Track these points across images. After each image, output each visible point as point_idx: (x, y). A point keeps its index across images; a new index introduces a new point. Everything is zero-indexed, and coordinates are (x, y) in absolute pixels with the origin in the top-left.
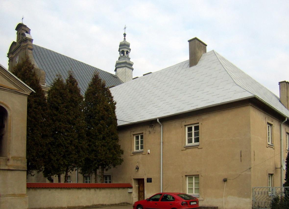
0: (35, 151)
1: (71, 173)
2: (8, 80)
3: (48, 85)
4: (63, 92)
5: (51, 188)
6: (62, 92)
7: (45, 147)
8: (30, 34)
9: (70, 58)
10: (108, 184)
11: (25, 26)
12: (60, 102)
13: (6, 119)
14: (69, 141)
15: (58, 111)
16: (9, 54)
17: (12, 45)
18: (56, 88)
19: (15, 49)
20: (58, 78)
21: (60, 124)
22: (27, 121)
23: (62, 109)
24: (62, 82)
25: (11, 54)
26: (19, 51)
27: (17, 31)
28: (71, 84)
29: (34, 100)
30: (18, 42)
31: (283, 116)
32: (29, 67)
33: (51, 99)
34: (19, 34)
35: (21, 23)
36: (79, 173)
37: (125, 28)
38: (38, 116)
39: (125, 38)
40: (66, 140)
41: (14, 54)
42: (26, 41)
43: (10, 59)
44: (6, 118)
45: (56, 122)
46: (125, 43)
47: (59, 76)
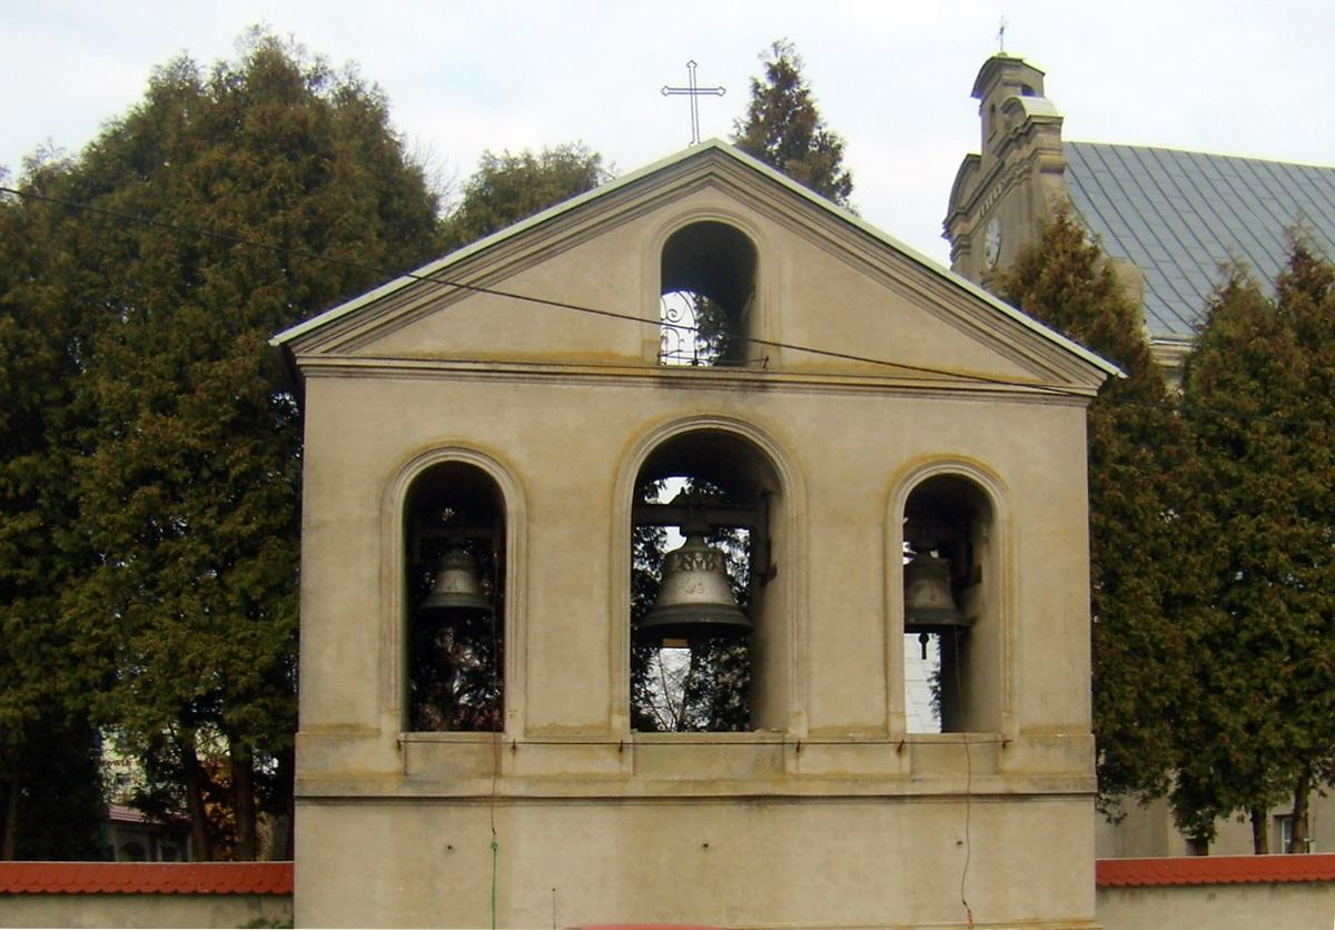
0: (1129, 688)
1: (1322, 794)
3: (1159, 334)
4: (1265, 347)
5: (1220, 884)
6: (1259, 351)
7: (1181, 663)
8: (1041, 94)
9: (1264, 164)
11: (1018, 64)
12: (1253, 406)
13: (987, 540)
14: (1313, 617)
15: (1242, 460)
16: (949, 224)
18: (1220, 336)
19: (979, 188)
20: (1227, 281)
21: (1259, 530)
23: (1265, 442)
24: (1253, 292)
25: (959, 217)
26: (999, 196)
27: (979, 102)
28: (1305, 294)
29: (1115, 421)
30: (992, 150)
32: (1074, 255)
33: (1201, 400)
34: (993, 108)
35: (995, 55)
36: (1199, 844)
38: (1140, 500)
40: (1295, 609)
41: (976, 212)
42: (1027, 133)
43: (957, 243)
44: (988, 531)
45: (1235, 520)
47: (1231, 266)
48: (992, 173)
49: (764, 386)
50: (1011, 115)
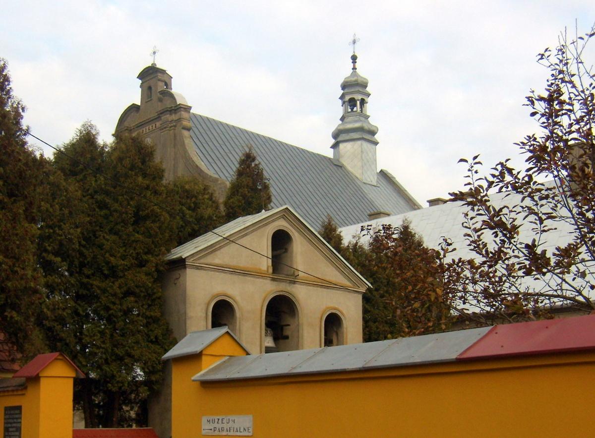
2: (342, 273)
10: (135, 430)
11: (163, 72)
17: (129, 110)
27: (140, 81)
37: (354, 42)
39: (354, 66)
42: (175, 110)
46: (356, 81)
48: (150, 120)
49: (294, 282)
50: (164, 96)
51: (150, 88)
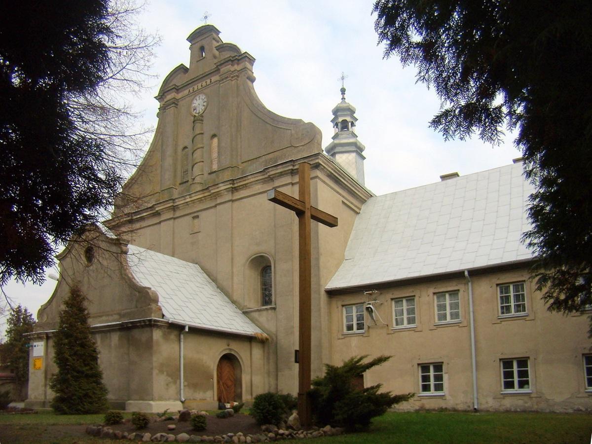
17: (175, 72)
22: (311, 305)
25: (174, 90)
27: (191, 44)
31: (516, 264)
37: (343, 78)
39: (343, 96)
51: (202, 49)
